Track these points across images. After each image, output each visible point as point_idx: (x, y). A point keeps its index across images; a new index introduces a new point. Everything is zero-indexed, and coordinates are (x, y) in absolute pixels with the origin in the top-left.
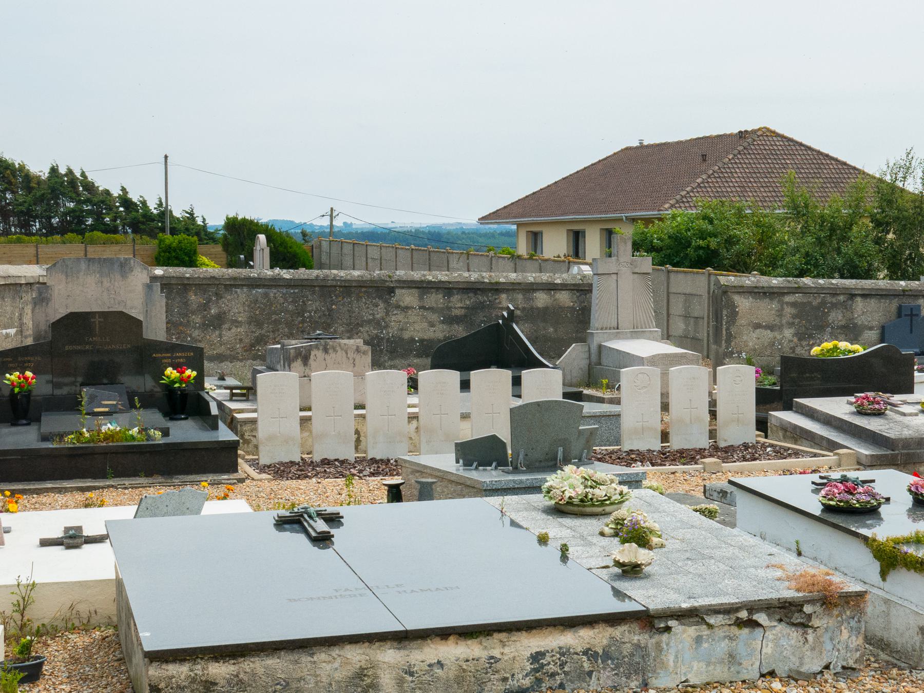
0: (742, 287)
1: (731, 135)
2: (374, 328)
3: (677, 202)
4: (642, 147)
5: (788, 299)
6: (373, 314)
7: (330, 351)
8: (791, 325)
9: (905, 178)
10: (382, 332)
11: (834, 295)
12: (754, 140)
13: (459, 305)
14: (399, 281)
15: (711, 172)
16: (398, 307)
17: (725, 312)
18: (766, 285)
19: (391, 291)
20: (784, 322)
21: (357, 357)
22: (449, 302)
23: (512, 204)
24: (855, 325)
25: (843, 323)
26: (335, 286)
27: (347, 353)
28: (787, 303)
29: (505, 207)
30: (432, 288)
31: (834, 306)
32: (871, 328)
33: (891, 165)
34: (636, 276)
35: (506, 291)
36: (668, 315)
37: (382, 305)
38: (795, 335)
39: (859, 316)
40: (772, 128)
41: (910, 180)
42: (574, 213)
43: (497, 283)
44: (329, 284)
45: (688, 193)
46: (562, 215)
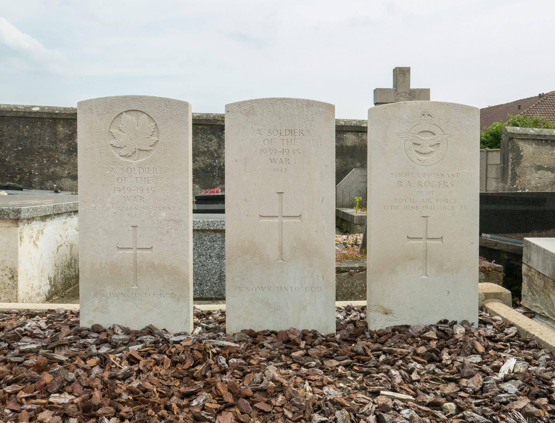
0: (526, 135)
1: (535, 97)
2: (208, 158)
4: (490, 108)
10: (215, 162)
15: (522, 113)
17: (510, 156)
18: (548, 134)
36: (487, 178)
37: (215, 140)
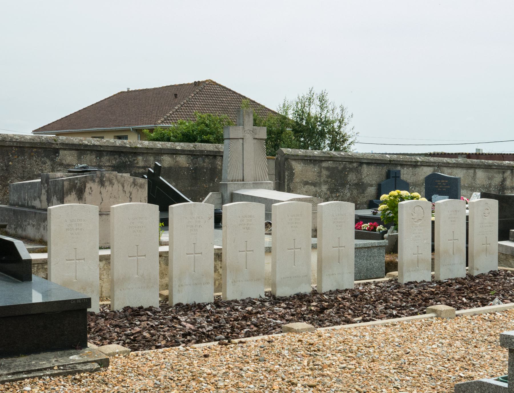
0: (297, 155)
3: (165, 120)
4: (129, 92)
5: (324, 164)
6: (42, 170)
7: (107, 184)
8: (326, 182)
9: (310, 105)
11: (351, 162)
12: (205, 87)
13: (108, 164)
14: (62, 144)
15: (182, 103)
16: (61, 164)
17: (286, 173)
19: (56, 151)
20: (322, 180)
21: (134, 191)
22: (101, 161)
23: (53, 122)
24: (363, 183)
25: (356, 182)
26: (12, 147)
27: (123, 187)
28: (324, 167)
29: (49, 124)
30: (88, 150)
31: (351, 170)
32: (371, 186)
33: (300, 98)
34: (256, 141)
35: (142, 154)
37: (49, 163)
38: (328, 189)
39: (365, 177)
40: (214, 80)
41: (312, 106)
42: (97, 127)
43: (136, 148)
44: (8, 144)
45: (171, 115)
46: (89, 128)
